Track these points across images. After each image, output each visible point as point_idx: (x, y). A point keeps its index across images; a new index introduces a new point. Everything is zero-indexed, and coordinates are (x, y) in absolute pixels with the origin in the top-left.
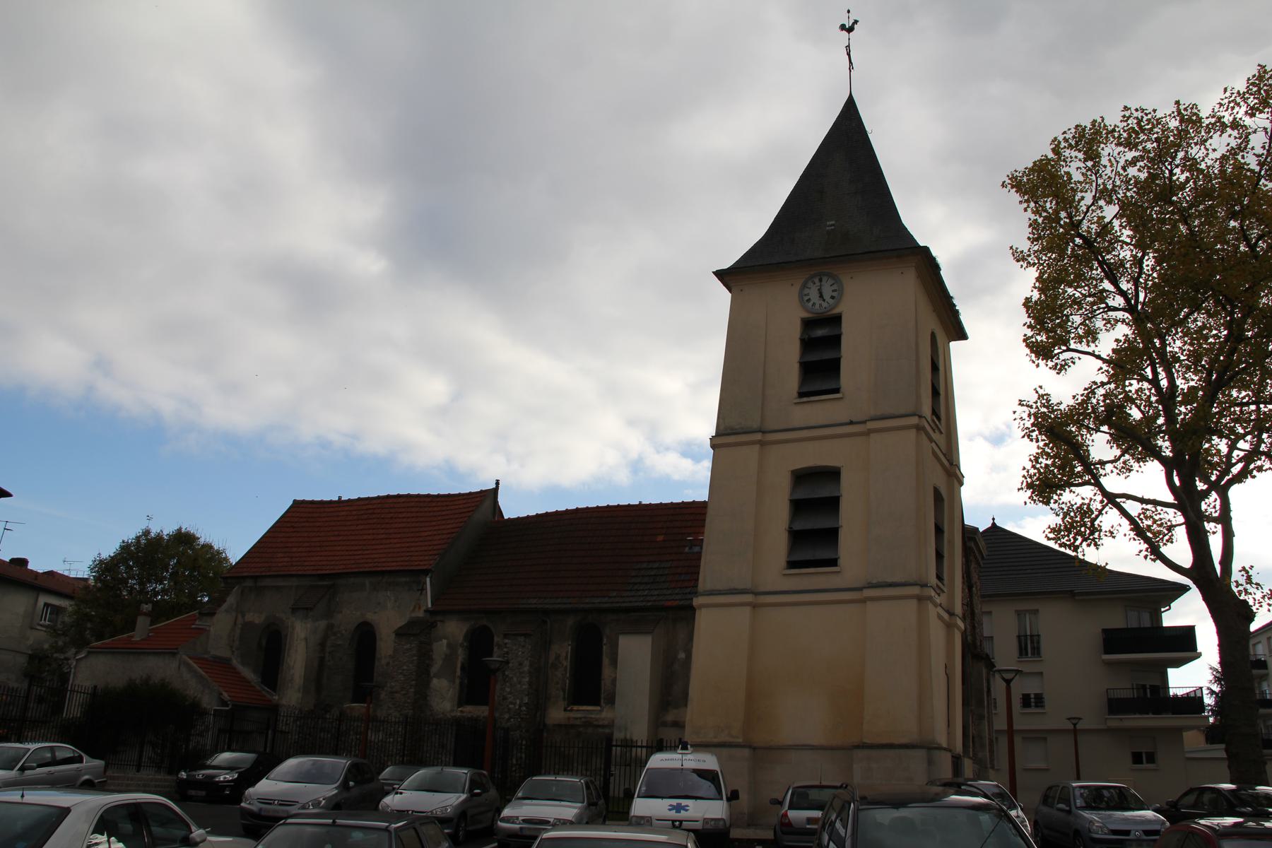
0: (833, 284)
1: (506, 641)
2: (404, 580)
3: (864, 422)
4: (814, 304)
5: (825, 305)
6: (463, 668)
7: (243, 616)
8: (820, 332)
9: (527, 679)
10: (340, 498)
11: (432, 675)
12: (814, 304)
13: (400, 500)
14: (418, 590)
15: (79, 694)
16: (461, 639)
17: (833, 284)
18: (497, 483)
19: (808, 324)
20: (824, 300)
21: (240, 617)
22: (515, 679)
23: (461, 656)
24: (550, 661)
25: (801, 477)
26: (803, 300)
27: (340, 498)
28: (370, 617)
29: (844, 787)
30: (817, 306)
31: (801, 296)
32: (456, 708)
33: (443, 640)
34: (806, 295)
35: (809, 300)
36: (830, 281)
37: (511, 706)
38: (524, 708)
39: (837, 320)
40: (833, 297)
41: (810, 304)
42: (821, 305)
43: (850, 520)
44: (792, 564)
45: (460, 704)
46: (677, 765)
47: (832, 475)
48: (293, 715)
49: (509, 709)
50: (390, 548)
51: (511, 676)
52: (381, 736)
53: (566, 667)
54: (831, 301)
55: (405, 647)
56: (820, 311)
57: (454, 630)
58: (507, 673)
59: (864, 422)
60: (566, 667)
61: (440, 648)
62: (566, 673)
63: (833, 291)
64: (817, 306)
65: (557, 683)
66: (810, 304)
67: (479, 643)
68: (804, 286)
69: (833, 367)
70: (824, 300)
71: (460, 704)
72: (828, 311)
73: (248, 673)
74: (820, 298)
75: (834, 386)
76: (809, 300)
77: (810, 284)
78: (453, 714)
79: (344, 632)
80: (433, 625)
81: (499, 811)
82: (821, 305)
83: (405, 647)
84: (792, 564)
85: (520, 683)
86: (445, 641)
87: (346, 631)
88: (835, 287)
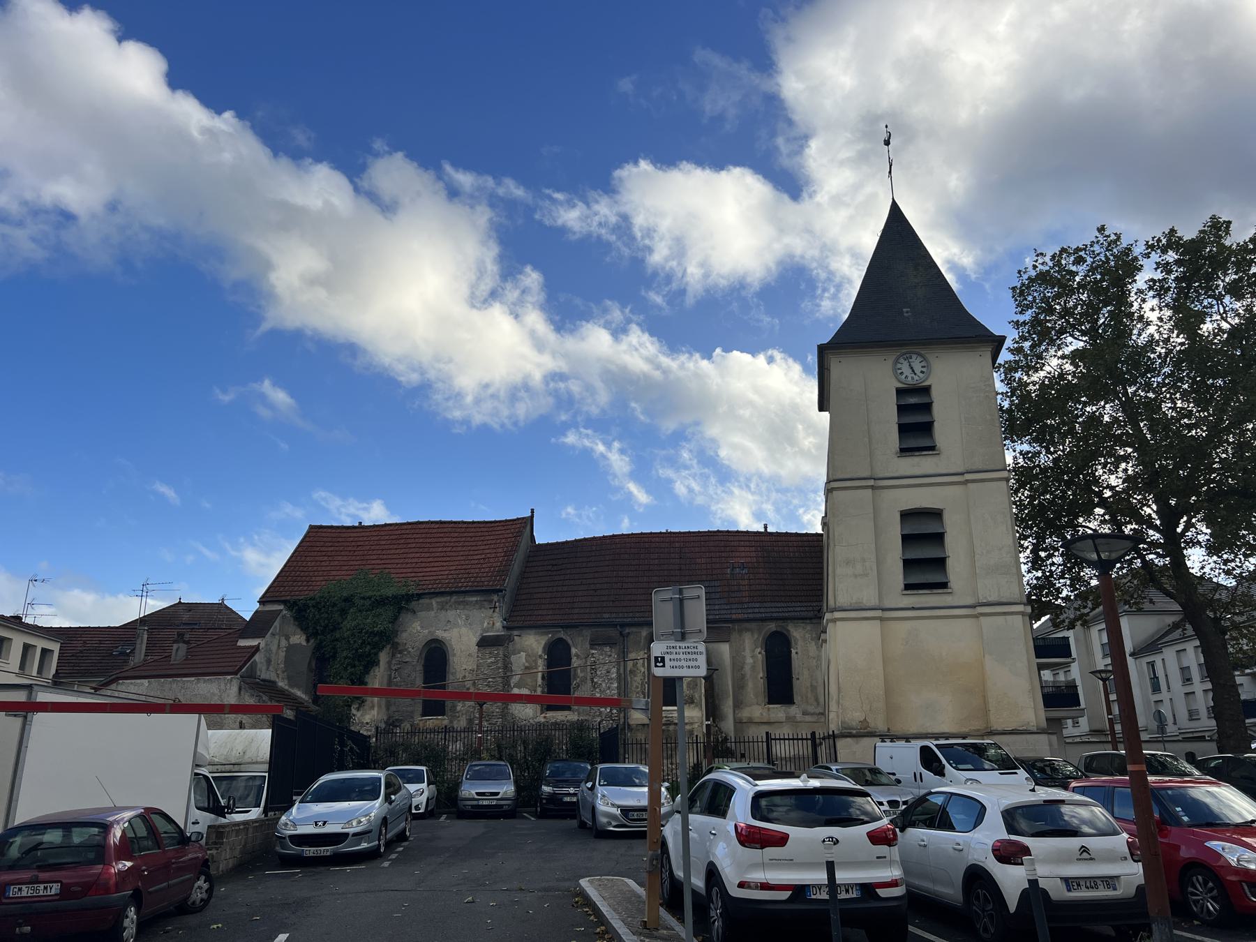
0: (922, 361)
2: (474, 599)
3: (962, 474)
4: (906, 377)
5: (916, 378)
8: (913, 400)
9: (616, 685)
10: (667, 530)
11: (512, 685)
12: (906, 377)
13: (387, 528)
14: (491, 608)
17: (922, 361)
18: (532, 511)
19: (900, 392)
20: (915, 374)
21: (283, 640)
22: (604, 685)
23: (541, 666)
24: (629, 669)
25: (907, 516)
26: (897, 373)
27: (667, 530)
28: (440, 634)
30: (910, 379)
31: (895, 370)
33: (522, 653)
34: (899, 369)
35: (902, 373)
36: (920, 359)
39: (926, 390)
40: (922, 372)
41: (903, 377)
42: (913, 378)
43: (955, 549)
44: (908, 587)
47: (935, 515)
48: (383, 732)
50: (430, 571)
52: (458, 746)
53: (644, 672)
54: (921, 375)
55: (489, 661)
56: (912, 383)
57: (533, 644)
58: (595, 680)
59: (962, 474)
60: (644, 672)
61: (519, 661)
62: (644, 679)
63: (923, 367)
64: (910, 379)
65: (637, 687)
66: (903, 377)
67: (557, 654)
68: (897, 361)
69: (927, 428)
70: (915, 374)
72: (924, 381)
74: (912, 371)
75: (927, 443)
76: (902, 373)
77: (902, 360)
79: (410, 649)
80: (510, 639)
81: (1199, 875)
82: (913, 378)
83: (489, 661)
84: (908, 587)
85: (609, 688)
88: (923, 364)
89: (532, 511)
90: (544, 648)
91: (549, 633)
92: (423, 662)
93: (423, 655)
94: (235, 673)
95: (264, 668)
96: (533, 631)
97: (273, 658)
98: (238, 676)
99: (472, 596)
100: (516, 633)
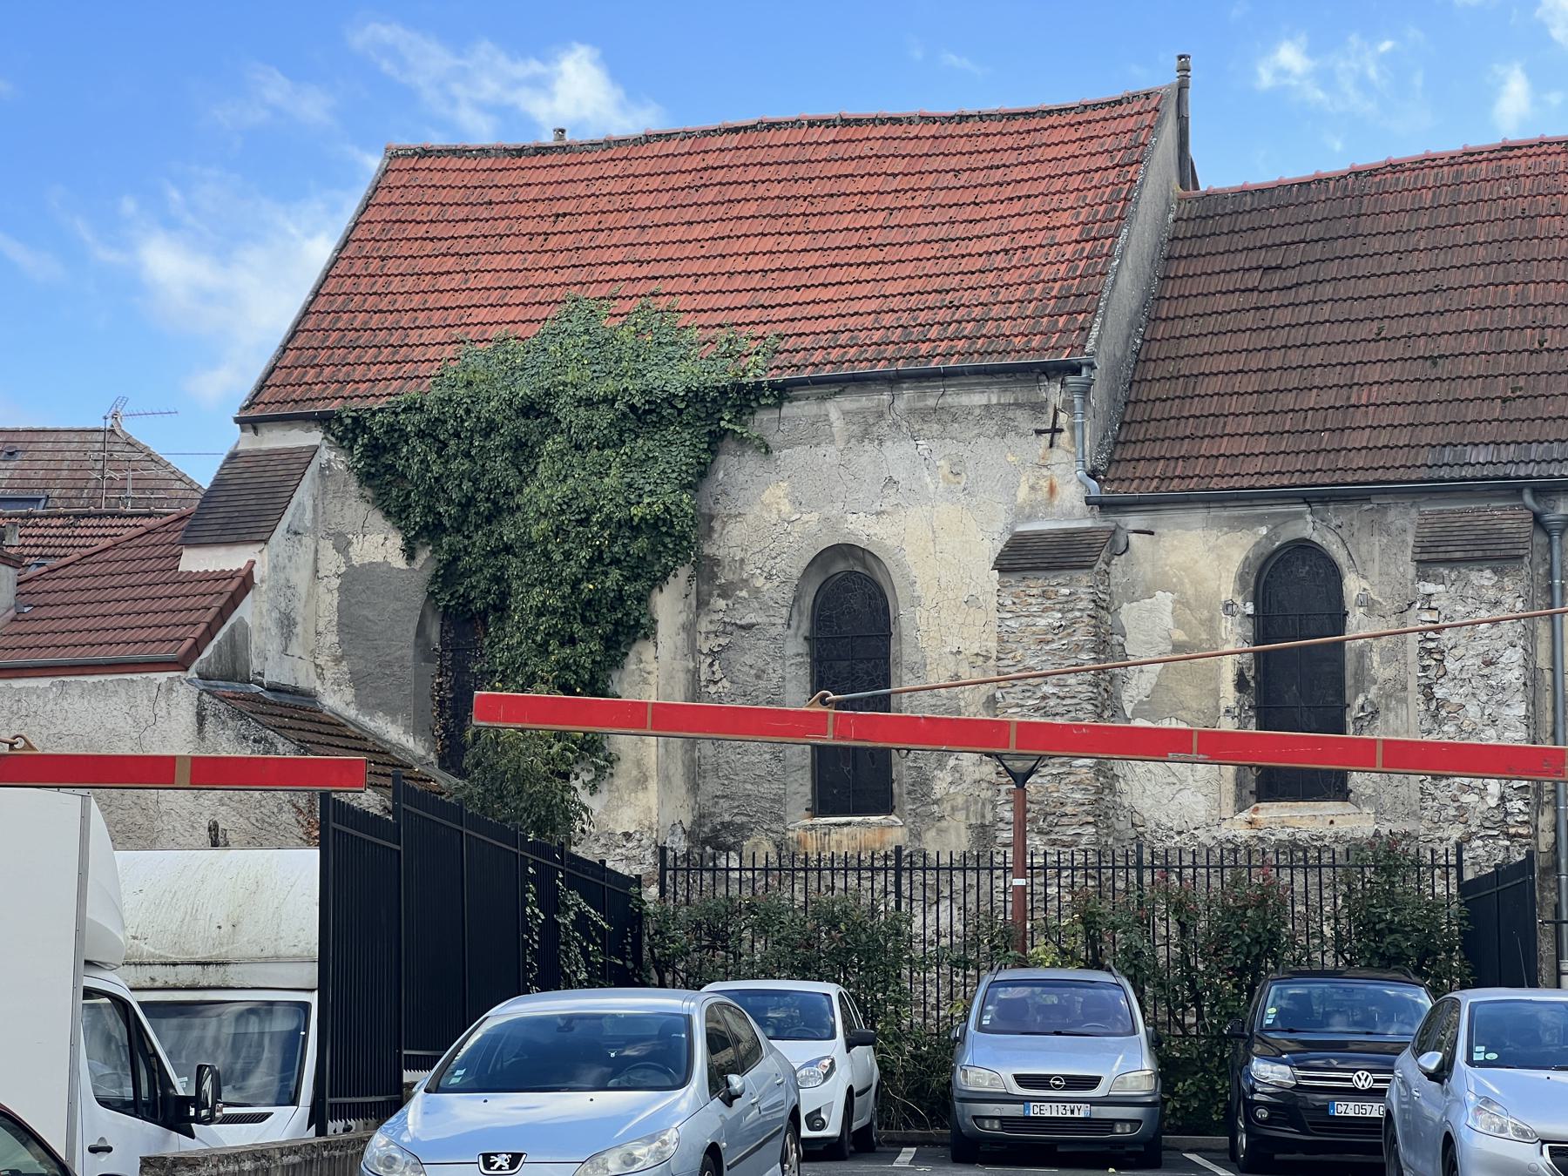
1: (1430, 588)
6: (1241, 684)
7: (343, 546)
9: (1521, 710)
14: (1039, 432)
15: (984, 875)
16: (1227, 588)
18: (1184, 69)
22: (1473, 710)
28: (861, 529)
29: (112, 431)
32: (1228, 811)
33: (1159, 594)
37: (1466, 798)
38: (1520, 804)
45: (1241, 805)
46: (1020, 1114)
49: (1462, 809)
51: (1455, 700)
55: (1042, 622)
71: (1241, 805)
73: (396, 733)
78: (1223, 832)
79: (759, 582)
83: (1042, 622)
86: (1164, 599)
87: (769, 578)
89: (1184, 69)
90: (1241, 577)
91: (1261, 520)
92: (805, 627)
93: (808, 601)
94: (182, 664)
95: (274, 647)
96: (1198, 516)
97: (300, 611)
98: (192, 674)
99: (969, 388)
100: (1133, 521)
